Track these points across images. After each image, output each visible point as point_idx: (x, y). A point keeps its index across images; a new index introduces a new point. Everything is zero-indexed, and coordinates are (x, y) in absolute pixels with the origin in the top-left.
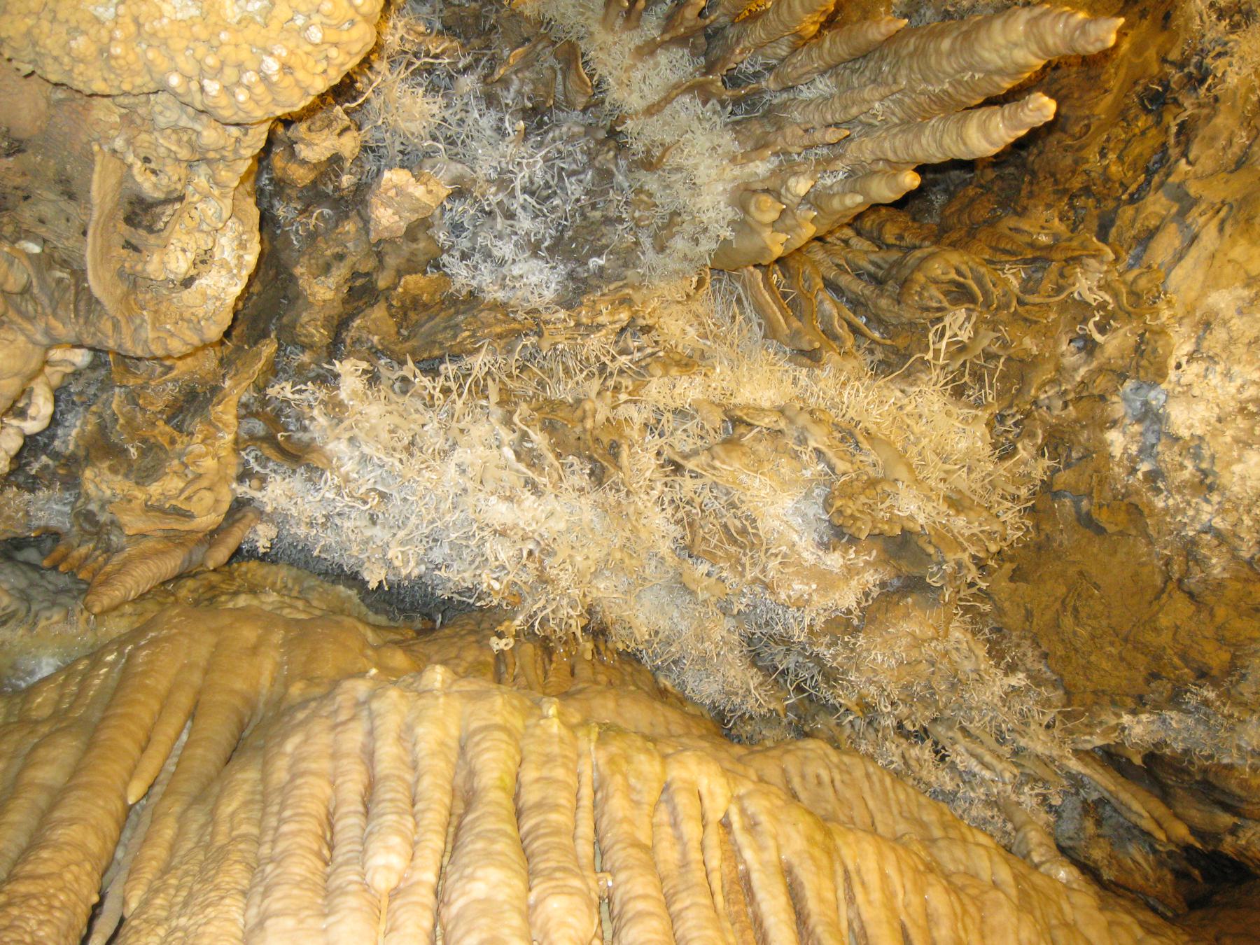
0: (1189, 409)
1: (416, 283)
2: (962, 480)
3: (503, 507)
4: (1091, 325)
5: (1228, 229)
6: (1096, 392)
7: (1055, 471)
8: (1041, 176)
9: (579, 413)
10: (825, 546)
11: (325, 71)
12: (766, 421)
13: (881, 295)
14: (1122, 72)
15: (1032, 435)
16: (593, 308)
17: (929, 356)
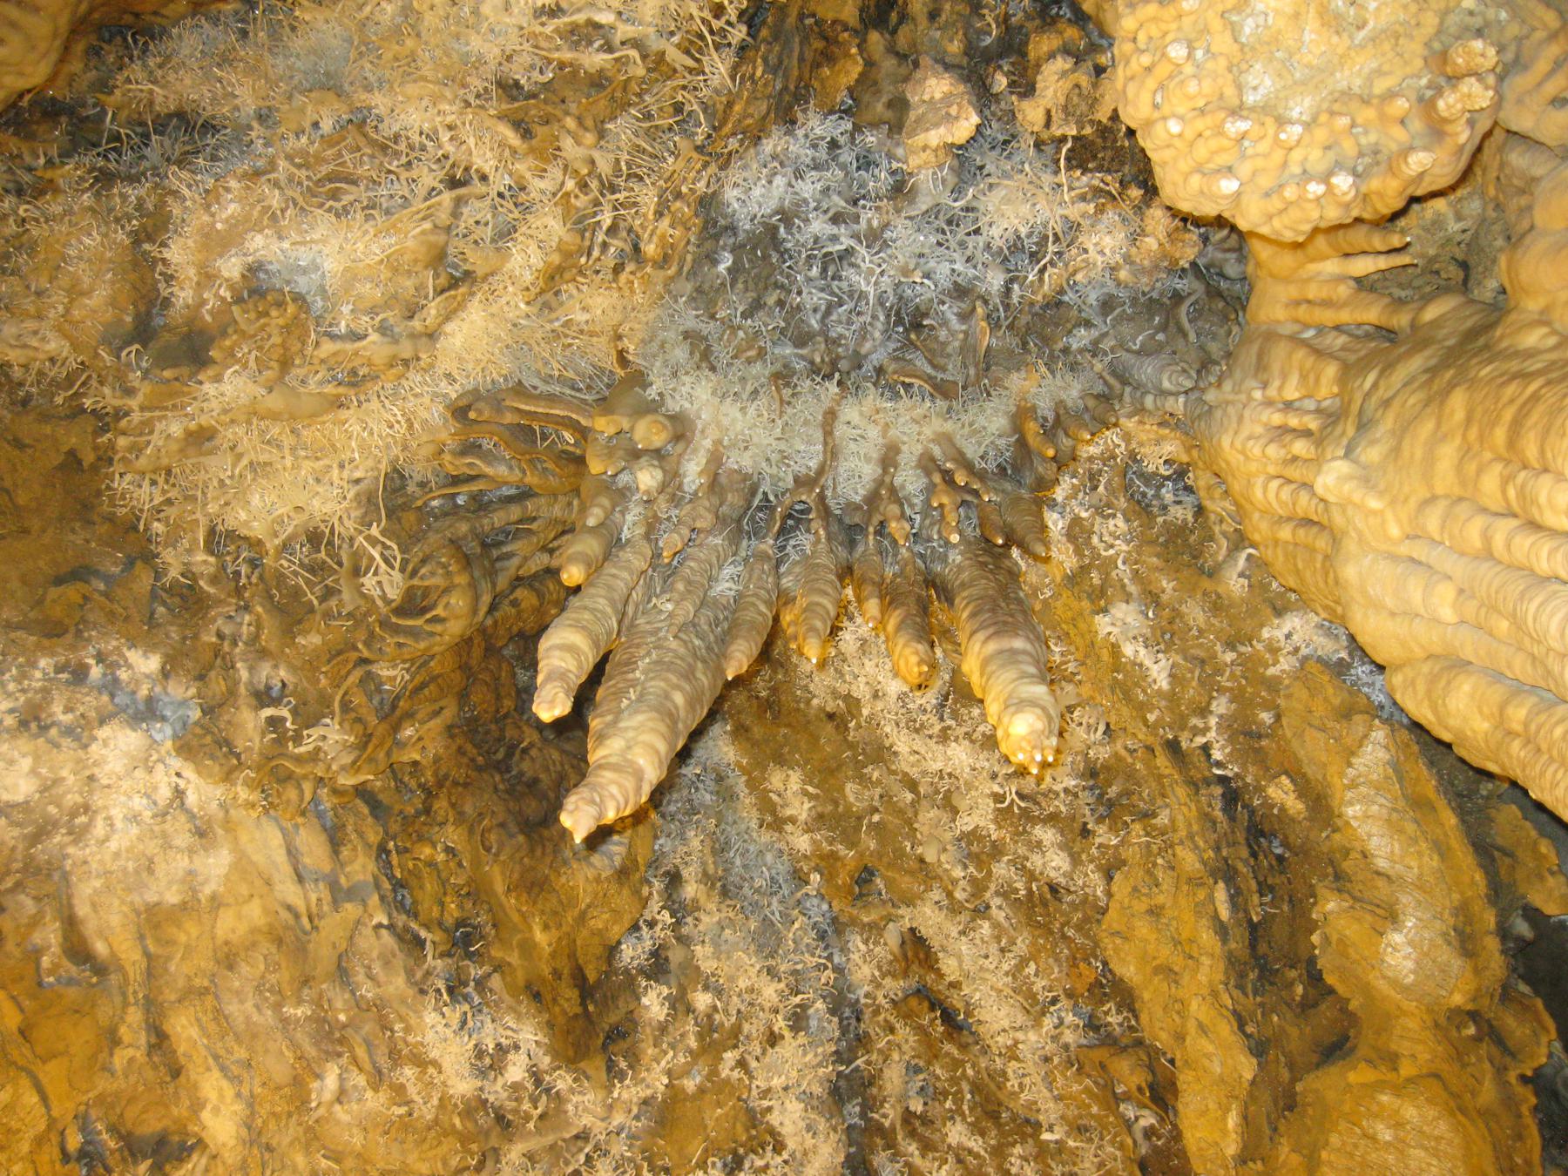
0: (127, 754)
1: (847, 73)
2: (219, 466)
5: (285, 915)
6: (213, 674)
7: (158, 576)
8: (473, 774)
9: (589, 123)
10: (253, 270)
11: (1134, 40)
12: (433, 310)
13: (473, 530)
14: (516, 917)
15: (214, 580)
16: (684, 224)
17: (375, 531)
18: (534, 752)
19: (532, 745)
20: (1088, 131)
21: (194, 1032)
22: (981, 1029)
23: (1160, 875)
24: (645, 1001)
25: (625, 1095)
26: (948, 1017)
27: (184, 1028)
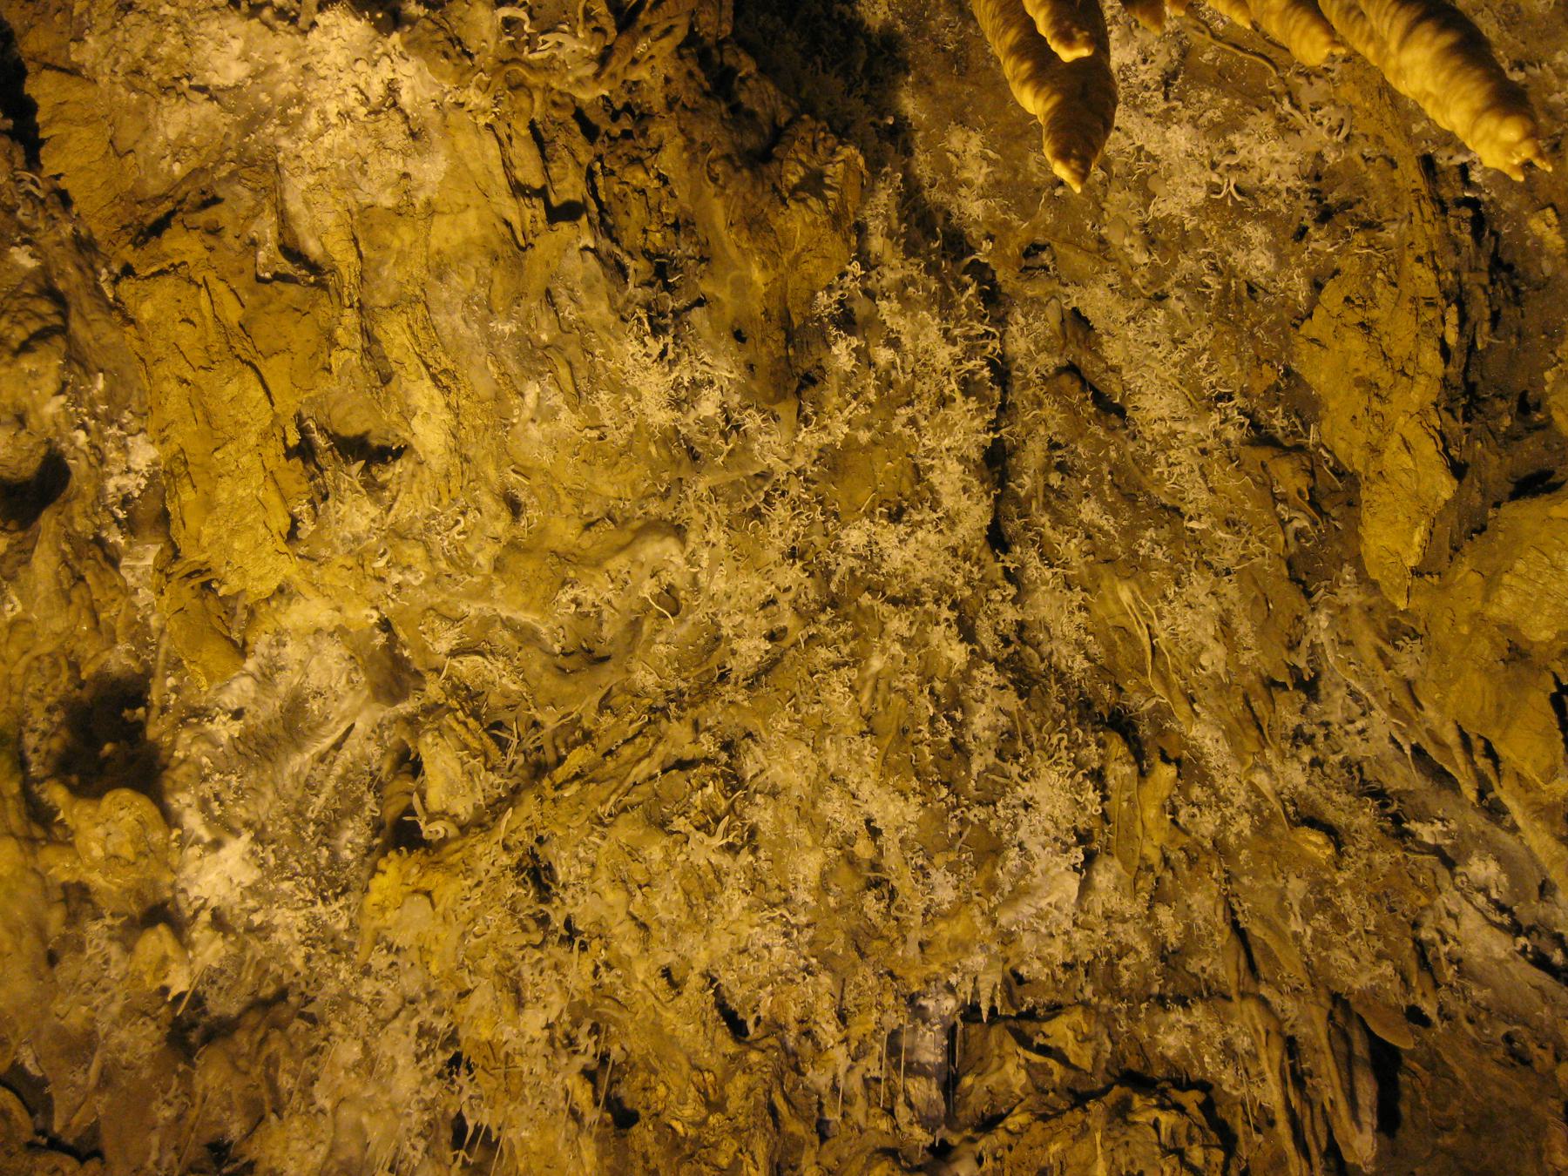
4: (522, 14)
8: (701, 100)
18: (751, 83)
19: (749, 75)
21: (405, 339)
22: (1137, 415)
23: (1378, 289)
24: (835, 350)
25: (808, 441)
26: (1100, 399)
27: (396, 336)
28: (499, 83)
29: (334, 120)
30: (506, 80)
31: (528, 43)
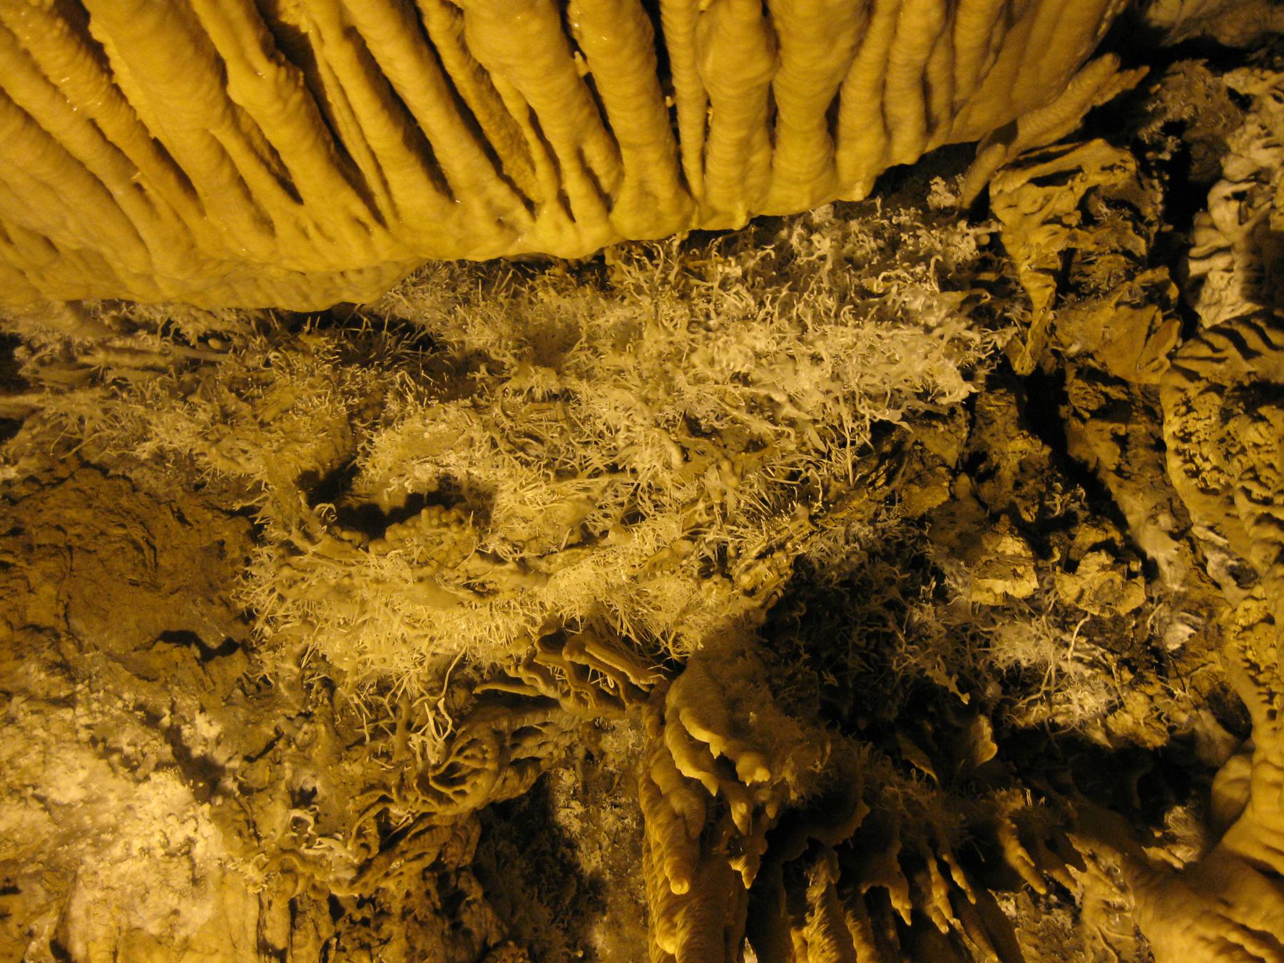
3: (760, 345)
4: (311, 820)
8: (431, 917)
15: (291, 687)
18: (475, 907)
19: (475, 900)
20: (1107, 615)
28: (274, 866)
29: (135, 852)
30: (281, 864)
31: (307, 840)
